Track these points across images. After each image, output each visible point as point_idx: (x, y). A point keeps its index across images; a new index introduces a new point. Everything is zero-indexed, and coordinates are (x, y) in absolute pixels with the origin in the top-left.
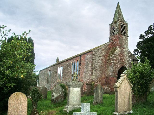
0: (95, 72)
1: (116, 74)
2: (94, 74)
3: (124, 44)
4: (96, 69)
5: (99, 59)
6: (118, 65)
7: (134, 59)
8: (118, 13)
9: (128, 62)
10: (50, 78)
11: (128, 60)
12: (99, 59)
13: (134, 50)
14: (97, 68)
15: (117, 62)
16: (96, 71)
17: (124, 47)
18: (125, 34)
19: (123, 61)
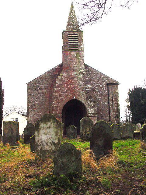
0: (33, 112)
1: (59, 113)
2: (30, 115)
3: (75, 64)
4: (35, 108)
5: (39, 93)
6: (62, 99)
7: (108, 83)
8: (72, 18)
9: (83, 91)
10: (109, 103)
11: (83, 88)
12: (39, 93)
13: (28, 84)
14: (36, 106)
15: (60, 95)
16: (33, 110)
17: (75, 68)
18: (77, 48)
19: (72, 91)
